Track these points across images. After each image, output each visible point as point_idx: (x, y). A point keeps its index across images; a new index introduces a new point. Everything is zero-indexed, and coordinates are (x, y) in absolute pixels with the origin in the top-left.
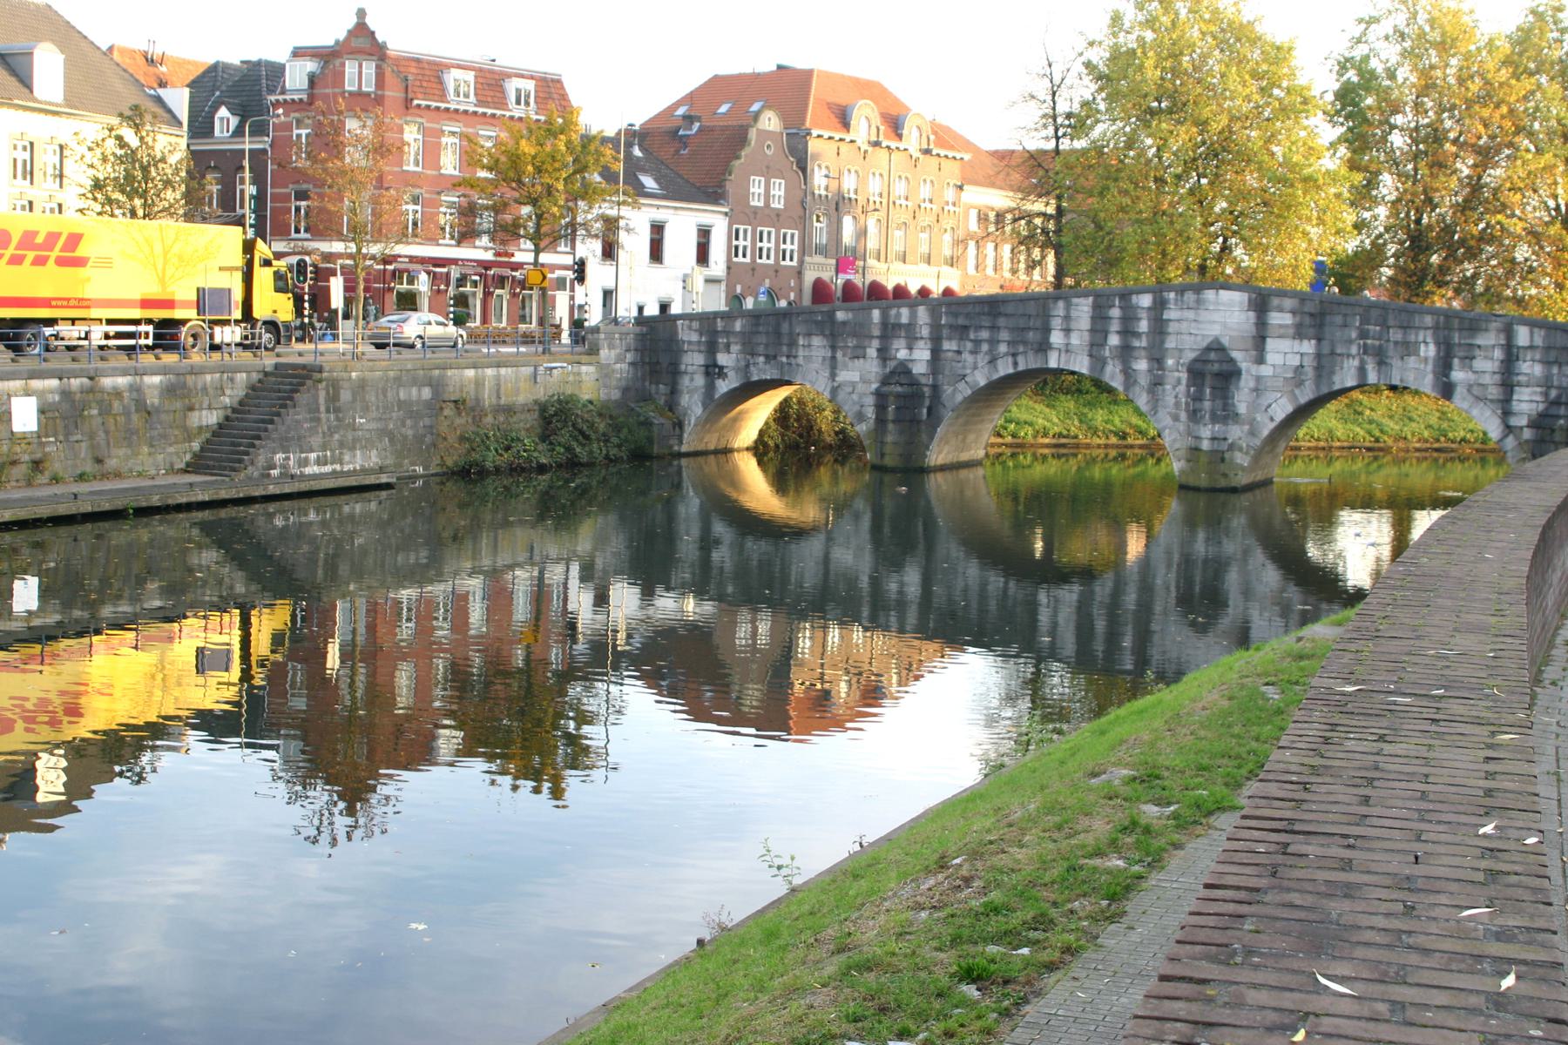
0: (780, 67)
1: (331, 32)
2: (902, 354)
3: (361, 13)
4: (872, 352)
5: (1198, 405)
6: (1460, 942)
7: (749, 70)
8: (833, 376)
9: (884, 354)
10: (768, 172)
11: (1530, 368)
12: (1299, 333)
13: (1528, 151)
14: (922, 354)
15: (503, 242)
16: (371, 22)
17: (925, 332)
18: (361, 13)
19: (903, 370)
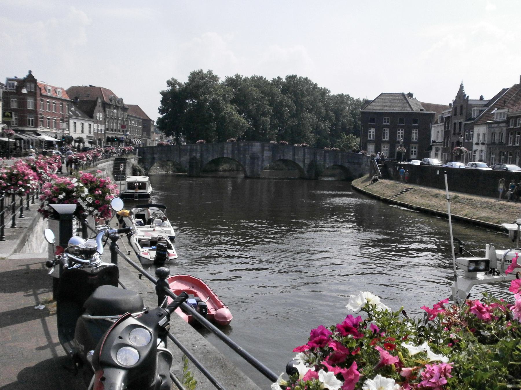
0: (90, 86)
1: (22, 75)
2: (194, 154)
3: (30, 72)
4: (188, 154)
5: (482, 154)
6: (280, 276)
7: (76, 86)
8: (180, 159)
9: (190, 155)
10: (99, 112)
11: (307, 156)
12: (269, 150)
13: (293, 122)
14: (199, 155)
15: (403, 145)
16: (33, 74)
17: (199, 150)
18: (30, 72)
19: (195, 158)
